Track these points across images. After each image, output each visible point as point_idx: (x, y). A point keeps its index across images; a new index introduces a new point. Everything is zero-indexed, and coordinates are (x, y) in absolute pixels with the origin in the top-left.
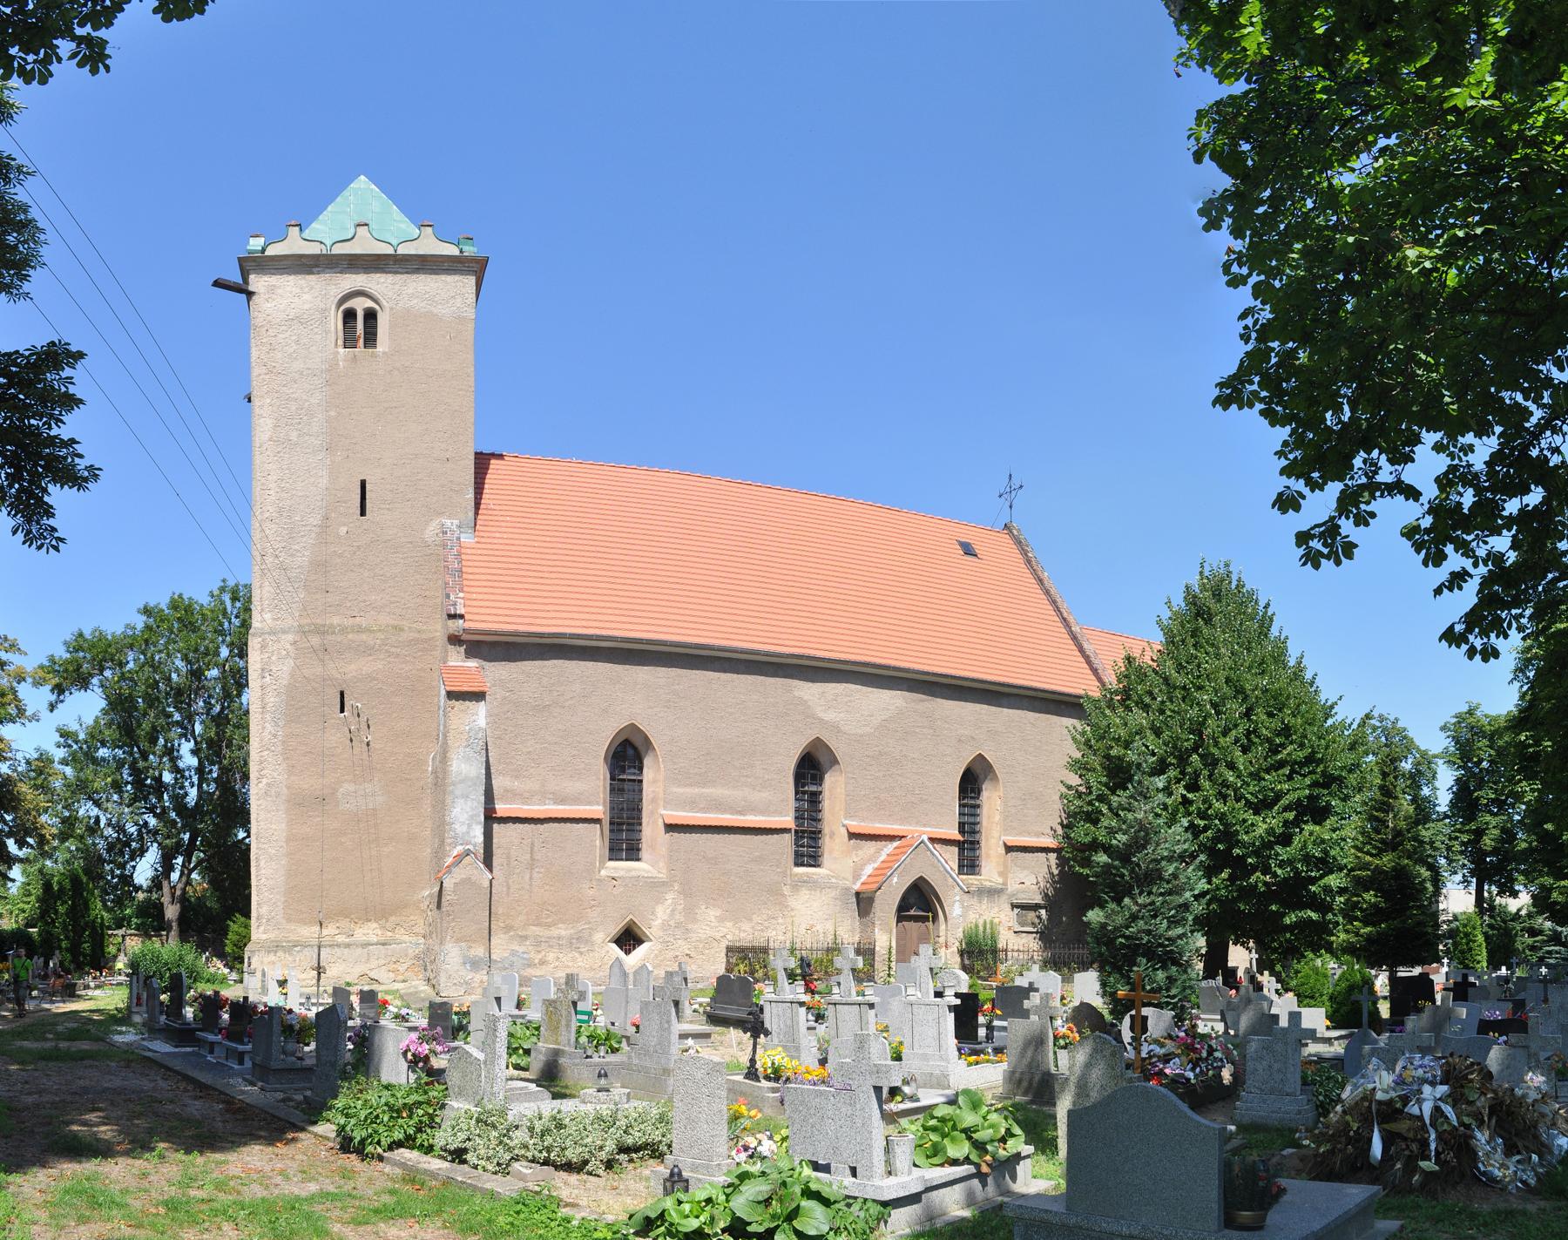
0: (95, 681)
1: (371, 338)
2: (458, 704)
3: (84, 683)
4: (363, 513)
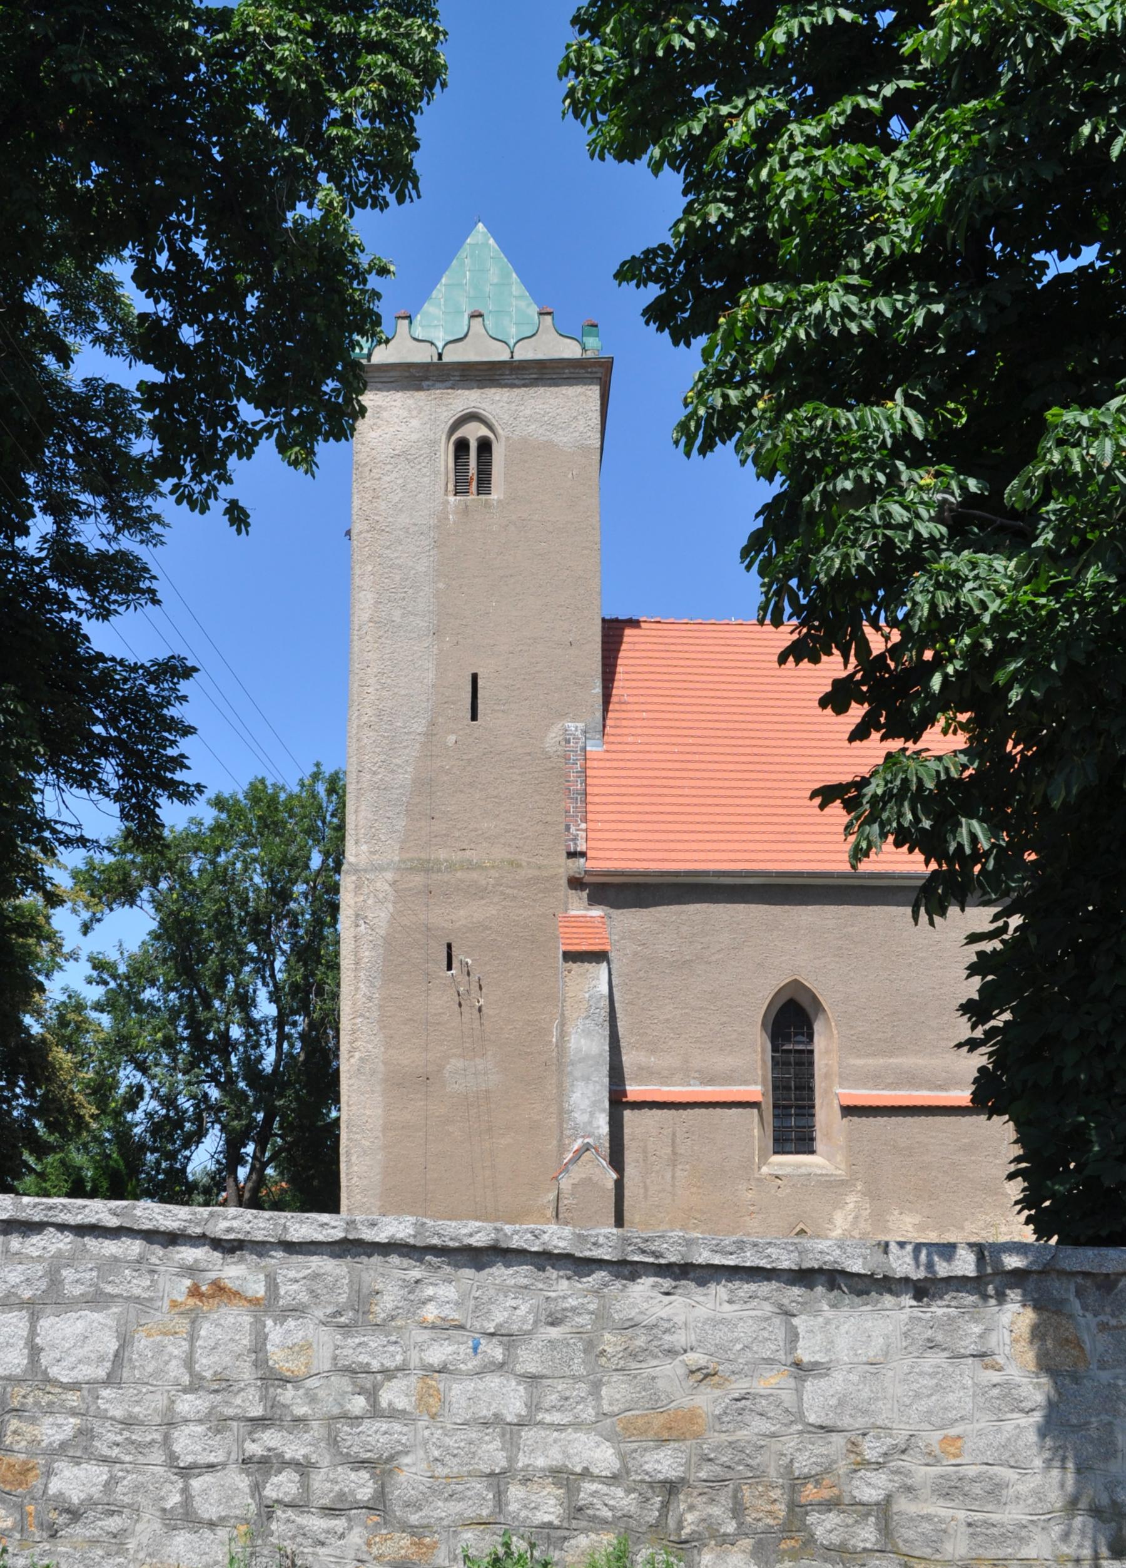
0: (145, 894)
1: (484, 481)
2: (575, 967)
3: (130, 897)
4: (474, 717)
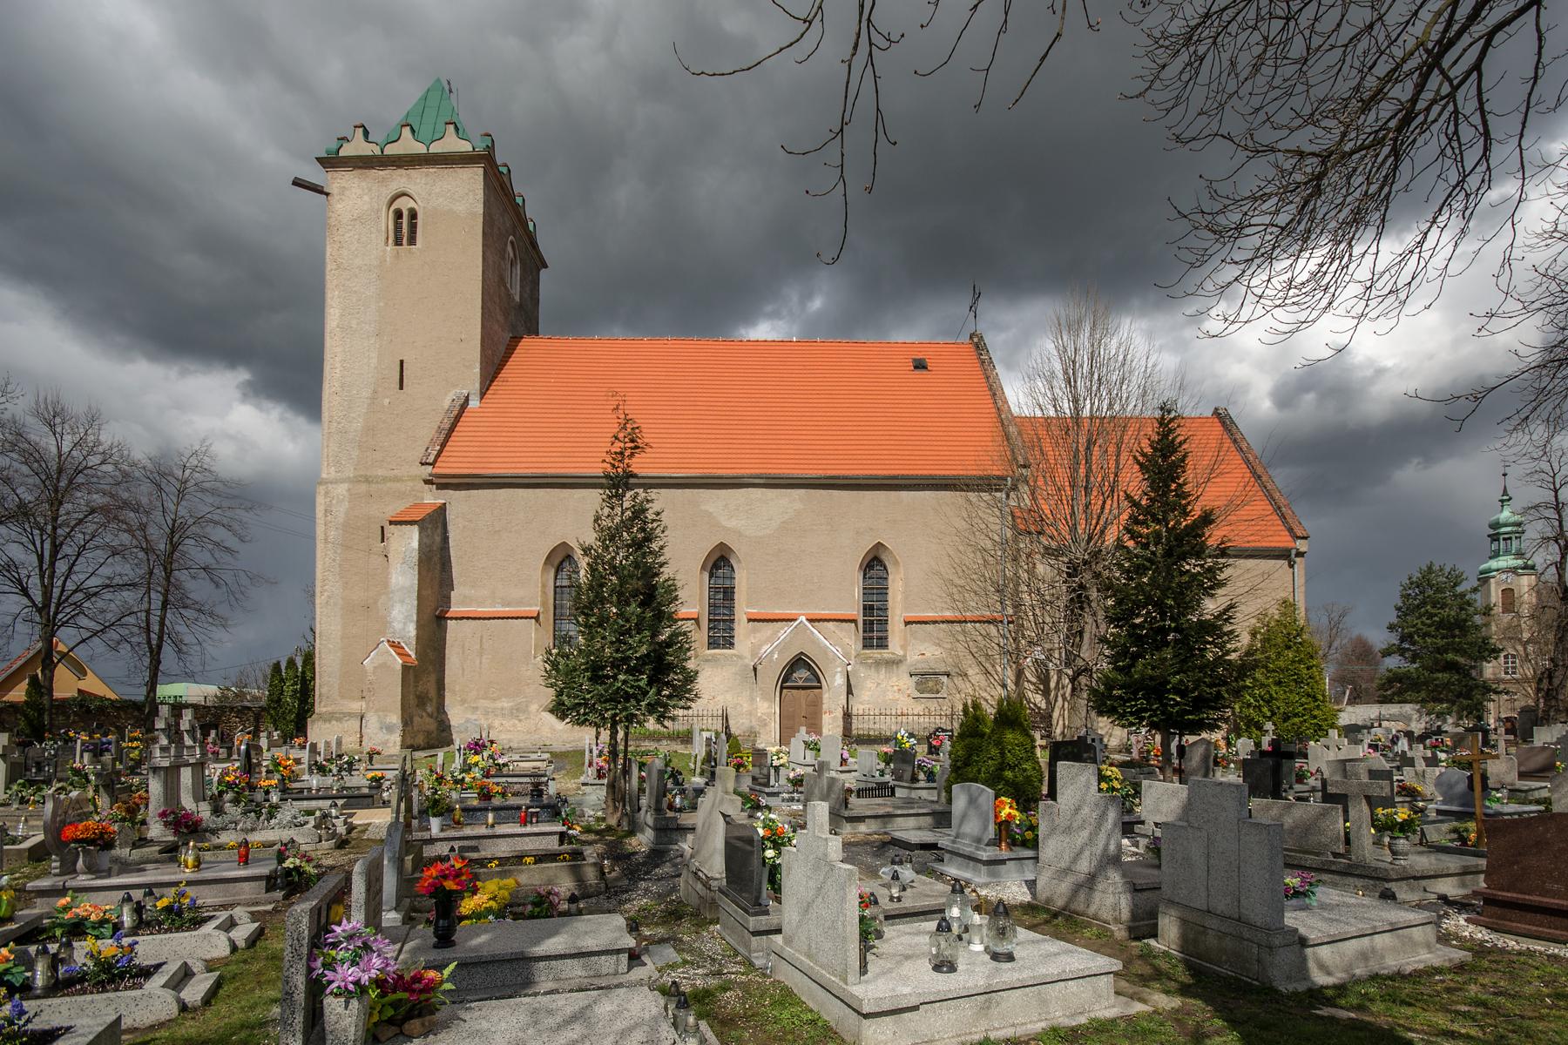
4: (401, 388)
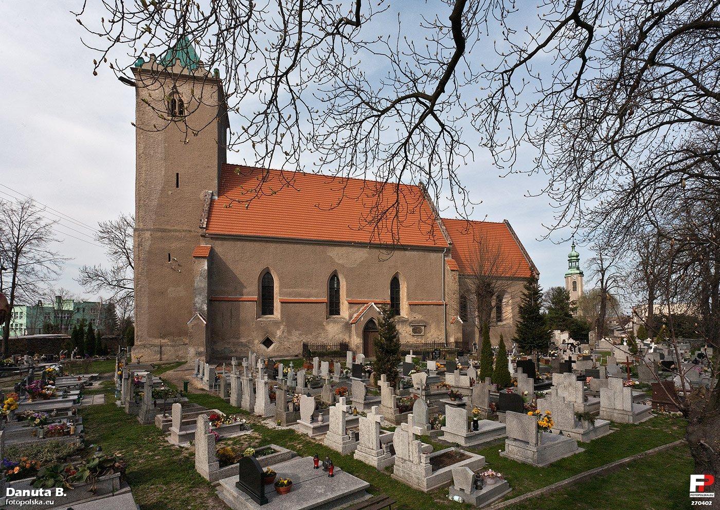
4: (177, 187)
